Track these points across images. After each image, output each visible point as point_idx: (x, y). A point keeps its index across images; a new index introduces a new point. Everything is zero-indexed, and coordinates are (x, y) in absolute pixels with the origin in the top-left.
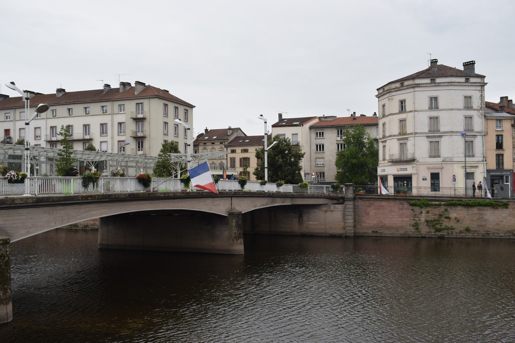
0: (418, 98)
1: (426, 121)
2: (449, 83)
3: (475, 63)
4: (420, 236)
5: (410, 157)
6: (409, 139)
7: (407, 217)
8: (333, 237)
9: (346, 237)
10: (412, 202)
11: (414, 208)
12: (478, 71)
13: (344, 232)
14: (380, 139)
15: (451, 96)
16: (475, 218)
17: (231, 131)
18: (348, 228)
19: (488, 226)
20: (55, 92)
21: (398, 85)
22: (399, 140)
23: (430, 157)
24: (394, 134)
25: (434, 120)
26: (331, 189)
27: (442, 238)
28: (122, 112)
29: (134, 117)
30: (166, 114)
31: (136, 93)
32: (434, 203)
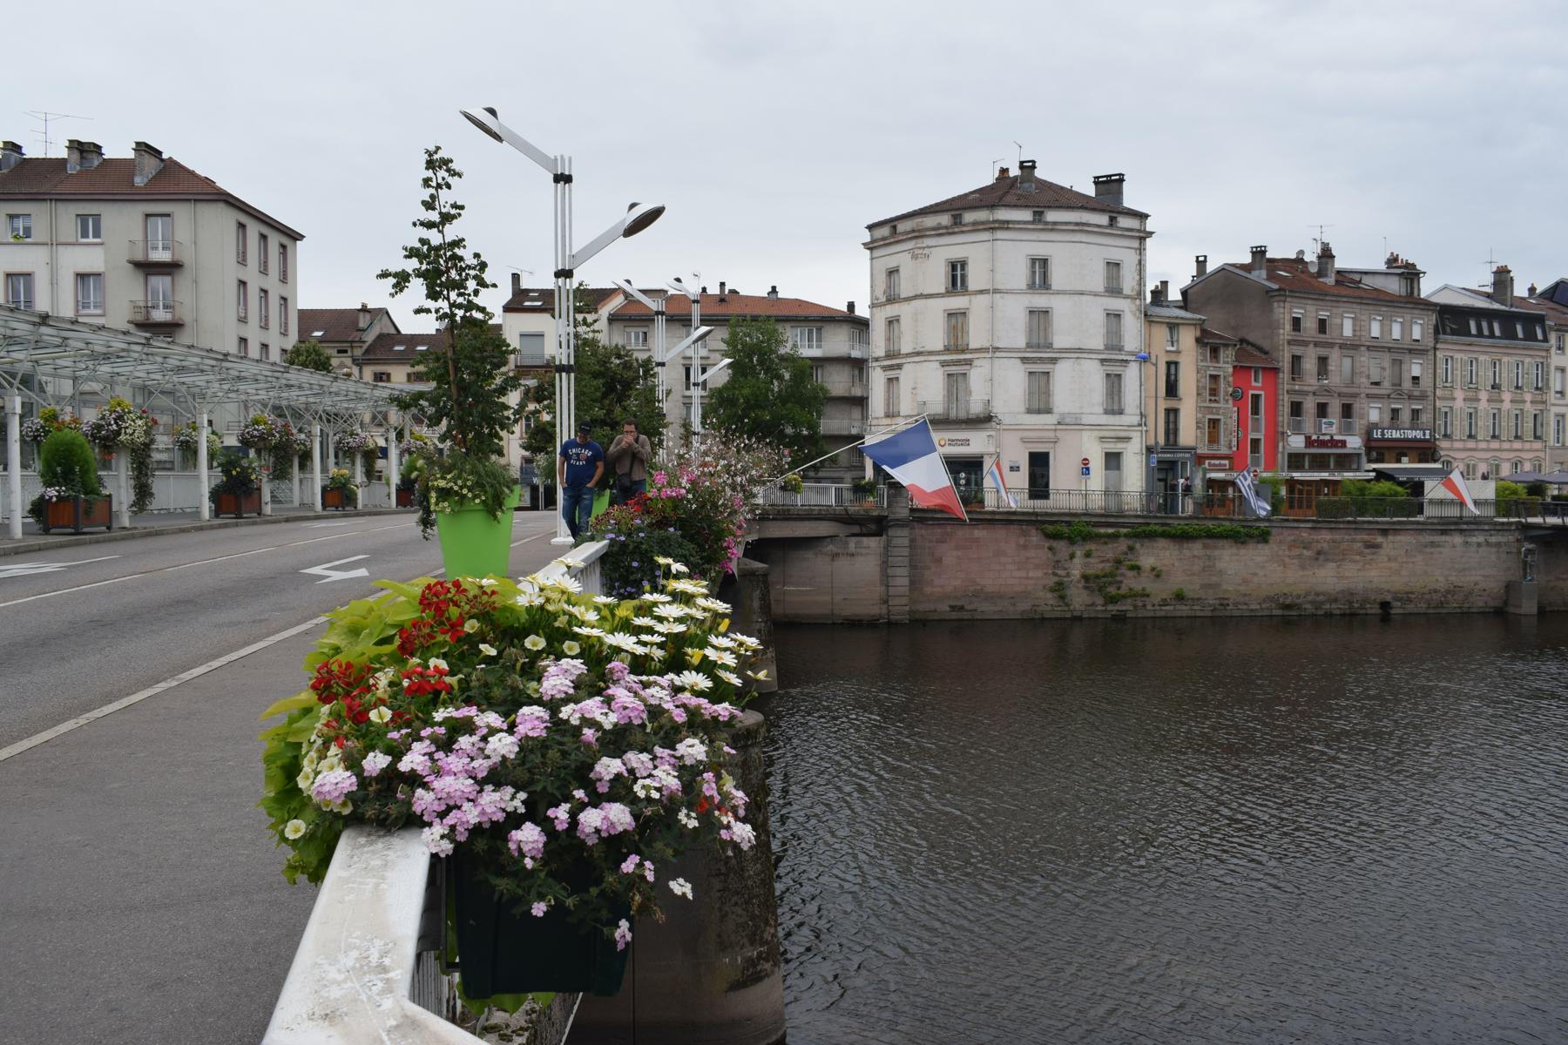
0: (1001, 259)
1: (1021, 318)
2: (1077, 224)
3: (1121, 180)
4: (1068, 615)
5: (976, 408)
6: (976, 363)
7: (1037, 567)
8: (855, 625)
9: (890, 624)
10: (1050, 528)
11: (1055, 544)
12: (1130, 200)
13: (884, 611)
14: (877, 359)
15: (1078, 260)
16: (1196, 568)
17: (368, 316)
18: (897, 601)
19: (1225, 587)
20: (131, 155)
21: (945, 219)
22: (944, 364)
23: (1029, 411)
24: (929, 348)
25: (1040, 317)
26: (847, 495)
27: (1120, 618)
28: (91, 240)
29: (139, 257)
30: (242, 260)
31: (139, 181)
32: (1102, 530)
